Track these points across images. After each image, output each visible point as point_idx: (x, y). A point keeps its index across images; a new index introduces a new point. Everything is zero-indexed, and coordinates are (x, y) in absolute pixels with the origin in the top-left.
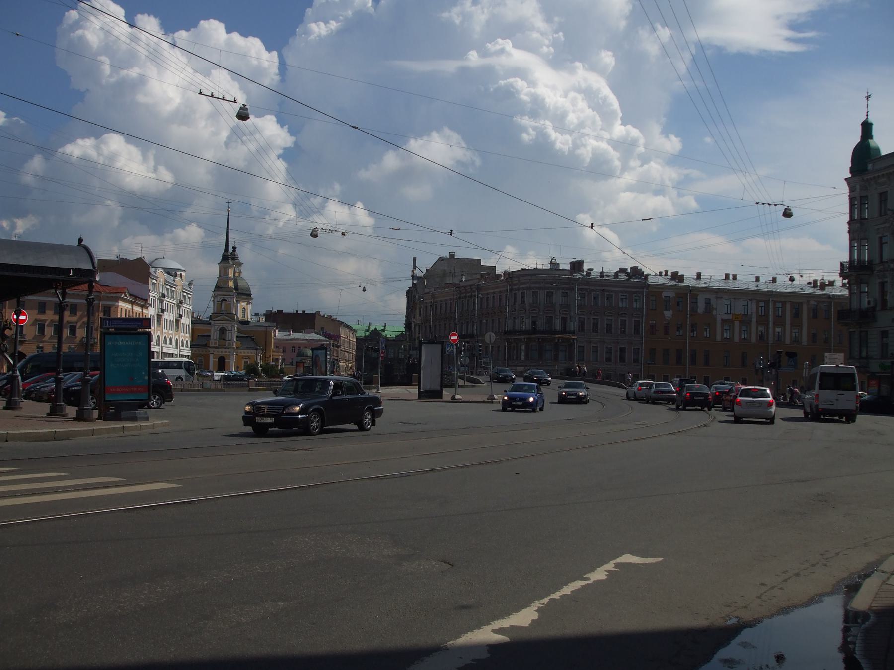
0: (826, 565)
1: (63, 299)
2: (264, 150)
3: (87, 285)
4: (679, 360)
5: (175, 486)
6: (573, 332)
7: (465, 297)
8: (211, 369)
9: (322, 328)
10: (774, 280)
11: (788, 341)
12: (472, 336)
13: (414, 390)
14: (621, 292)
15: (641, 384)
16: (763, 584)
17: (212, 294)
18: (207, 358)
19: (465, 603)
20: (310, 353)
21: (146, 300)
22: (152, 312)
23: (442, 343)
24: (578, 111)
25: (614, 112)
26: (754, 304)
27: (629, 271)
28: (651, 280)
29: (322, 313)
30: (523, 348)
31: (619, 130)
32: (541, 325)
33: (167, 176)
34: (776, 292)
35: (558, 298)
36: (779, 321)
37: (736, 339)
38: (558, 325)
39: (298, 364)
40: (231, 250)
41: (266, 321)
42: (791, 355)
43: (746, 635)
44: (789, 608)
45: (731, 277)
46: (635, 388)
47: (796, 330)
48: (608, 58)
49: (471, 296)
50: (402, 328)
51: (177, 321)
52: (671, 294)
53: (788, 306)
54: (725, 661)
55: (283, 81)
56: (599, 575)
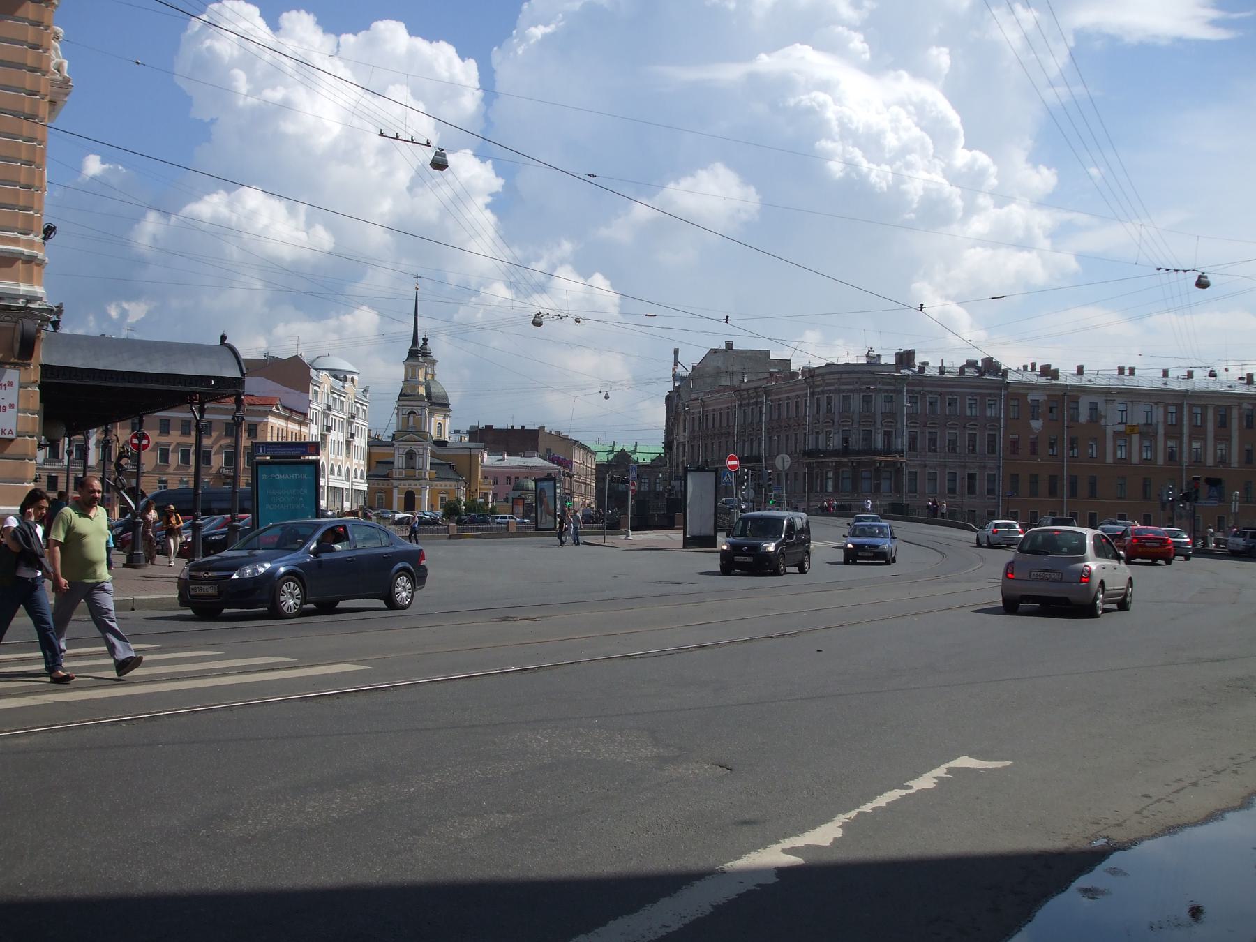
0: (1236, 772)
1: (202, 417)
2: (462, 196)
3: (233, 399)
4: (1053, 491)
5: (362, 667)
6: (901, 453)
7: (748, 404)
8: (395, 509)
9: (549, 450)
10: (1190, 375)
11: (1210, 461)
12: (758, 459)
13: (677, 536)
14: (971, 394)
15: (997, 525)
16: (1146, 796)
17: (395, 404)
18: (389, 493)
19: (747, 817)
20: (532, 485)
21: (305, 415)
22: (312, 432)
23: (716, 470)
24: (902, 131)
25: (954, 134)
26: (1161, 410)
27: (980, 364)
28: (1011, 377)
29: (547, 430)
30: (830, 474)
31: (961, 157)
32: (856, 442)
33: (324, 238)
34: (1193, 392)
35: (879, 405)
36: (1198, 432)
37: (1135, 460)
38: (879, 442)
39: (515, 501)
40: (421, 342)
41: (470, 441)
42: (1214, 482)
43: (1115, 859)
44: (1179, 826)
45: (1127, 372)
46: (989, 531)
47: (1223, 446)
48: (941, 57)
49: (756, 403)
50: (659, 448)
51: (348, 443)
52: (1041, 397)
53: (1210, 412)
54: (1085, 891)
55: (486, 117)
56: (926, 782)
